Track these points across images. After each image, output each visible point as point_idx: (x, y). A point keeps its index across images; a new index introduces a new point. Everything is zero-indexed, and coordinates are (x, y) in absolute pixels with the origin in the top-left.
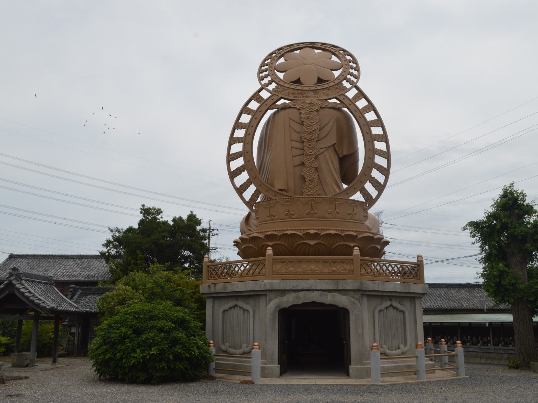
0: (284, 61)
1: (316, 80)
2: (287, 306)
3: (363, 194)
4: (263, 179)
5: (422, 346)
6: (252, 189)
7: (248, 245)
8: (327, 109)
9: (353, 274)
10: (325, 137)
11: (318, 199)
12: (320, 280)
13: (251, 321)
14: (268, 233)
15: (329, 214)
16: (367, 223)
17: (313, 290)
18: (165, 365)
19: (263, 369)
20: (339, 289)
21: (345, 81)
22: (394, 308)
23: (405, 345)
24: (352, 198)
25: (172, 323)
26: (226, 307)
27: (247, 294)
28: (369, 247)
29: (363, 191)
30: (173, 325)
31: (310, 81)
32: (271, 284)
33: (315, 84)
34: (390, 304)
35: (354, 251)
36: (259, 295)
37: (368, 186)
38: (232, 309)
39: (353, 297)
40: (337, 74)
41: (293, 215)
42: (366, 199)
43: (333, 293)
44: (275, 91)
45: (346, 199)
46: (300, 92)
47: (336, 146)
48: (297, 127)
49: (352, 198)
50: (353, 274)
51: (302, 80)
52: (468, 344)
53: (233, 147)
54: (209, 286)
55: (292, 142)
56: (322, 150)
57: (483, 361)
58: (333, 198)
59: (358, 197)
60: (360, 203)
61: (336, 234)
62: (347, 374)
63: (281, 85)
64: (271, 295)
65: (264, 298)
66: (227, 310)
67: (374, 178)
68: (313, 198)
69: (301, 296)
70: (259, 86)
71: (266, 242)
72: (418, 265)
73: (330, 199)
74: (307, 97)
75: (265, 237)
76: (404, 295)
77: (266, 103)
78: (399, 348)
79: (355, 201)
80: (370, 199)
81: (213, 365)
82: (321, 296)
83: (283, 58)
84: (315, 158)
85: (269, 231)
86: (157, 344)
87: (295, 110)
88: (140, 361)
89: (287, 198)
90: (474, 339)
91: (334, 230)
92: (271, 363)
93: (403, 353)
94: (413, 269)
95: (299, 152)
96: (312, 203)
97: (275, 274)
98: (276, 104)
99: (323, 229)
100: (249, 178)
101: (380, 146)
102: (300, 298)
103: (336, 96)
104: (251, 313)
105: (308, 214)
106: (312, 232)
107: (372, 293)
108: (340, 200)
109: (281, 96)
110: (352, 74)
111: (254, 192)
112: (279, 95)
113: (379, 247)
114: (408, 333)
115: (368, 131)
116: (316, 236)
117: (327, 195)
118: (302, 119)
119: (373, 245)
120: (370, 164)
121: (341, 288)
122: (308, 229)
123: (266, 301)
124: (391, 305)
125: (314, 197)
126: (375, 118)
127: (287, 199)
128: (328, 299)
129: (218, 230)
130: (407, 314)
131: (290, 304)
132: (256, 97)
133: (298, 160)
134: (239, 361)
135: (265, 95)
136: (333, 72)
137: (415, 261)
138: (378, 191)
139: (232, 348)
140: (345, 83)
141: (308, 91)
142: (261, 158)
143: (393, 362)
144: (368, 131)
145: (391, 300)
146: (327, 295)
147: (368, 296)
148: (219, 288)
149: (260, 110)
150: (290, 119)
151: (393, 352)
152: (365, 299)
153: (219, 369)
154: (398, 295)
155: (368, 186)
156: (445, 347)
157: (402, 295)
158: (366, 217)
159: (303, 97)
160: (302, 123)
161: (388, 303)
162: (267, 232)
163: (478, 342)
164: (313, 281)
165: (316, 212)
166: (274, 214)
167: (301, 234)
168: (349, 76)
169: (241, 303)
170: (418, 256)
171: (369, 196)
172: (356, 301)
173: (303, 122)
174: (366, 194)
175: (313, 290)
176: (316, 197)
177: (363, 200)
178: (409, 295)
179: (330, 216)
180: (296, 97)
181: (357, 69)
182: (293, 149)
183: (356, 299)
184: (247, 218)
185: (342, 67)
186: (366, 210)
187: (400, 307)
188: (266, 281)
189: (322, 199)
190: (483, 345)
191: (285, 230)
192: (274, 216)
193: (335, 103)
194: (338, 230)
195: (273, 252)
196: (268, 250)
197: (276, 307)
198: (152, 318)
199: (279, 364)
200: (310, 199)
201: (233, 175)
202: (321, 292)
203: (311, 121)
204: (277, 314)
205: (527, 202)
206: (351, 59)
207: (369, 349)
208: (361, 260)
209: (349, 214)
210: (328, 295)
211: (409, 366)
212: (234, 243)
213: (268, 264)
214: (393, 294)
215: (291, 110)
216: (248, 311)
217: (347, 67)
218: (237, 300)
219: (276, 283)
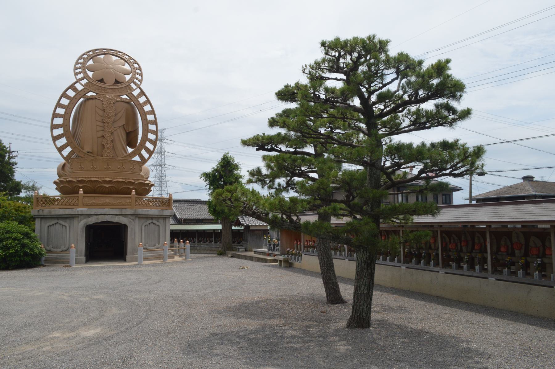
0: (93, 63)
1: (114, 81)
2: (91, 223)
4: (76, 143)
6: (68, 150)
7: (65, 185)
8: (120, 102)
9: (131, 205)
10: (118, 120)
13: (68, 232)
14: (79, 179)
16: (142, 173)
18: (18, 259)
19: (76, 259)
21: (133, 83)
22: (154, 224)
23: (159, 244)
24: (133, 159)
25: (22, 235)
26: (50, 224)
27: (66, 216)
30: (22, 236)
31: (110, 82)
32: (82, 211)
33: (113, 84)
36: (74, 217)
37: (144, 152)
38: (55, 225)
39: (130, 218)
40: (128, 77)
44: (86, 86)
46: (103, 89)
47: (125, 126)
48: (101, 112)
49: (133, 159)
50: (131, 205)
51: (105, 80)
52: (201, 242)
53: (55, 119)
54: (38, 211)
55: (97, 122)
56: (115, 129)
57: (208, 252)
59: (137, 158)
61: (122, 181)
62: (125, 260)
63: (90, 82)
64: (82, 217)
65: (76, 219)
66: (51, 226)
67: (147, 147)
70: (75, 80)
71: (78, 184)
72: (169, 200)
74: (107, 93)
75: (77, 181)
76: (160, 216)
77: (79, 93)
78: (155, 246)
79: (135, 161)
81: (43, 259)
83: (91, 60)
84: (111, 134)
85: (80, 178)
86: (14, 247)
87: (99, 101)
88: (3, 257)
90: (205, 239)
91: (121, 178)
92: (80, 256)
95: (102, 129)
97: (84, 205)
98: (87, 95)
100: (66, 142)
101: (152, 127)
103: (127, 94)
104: (68, 228)
106: (108, 179)
107: (141, 216)
109: (91, 90)
110: (137, 79)
112: (89, 89)
113: (147, 188)
114: (161, 237)
115: (145, 118)
116: (110, 182)
117: (118, 157)
118: (104, 108)
119: (143, 187)
120: (145, 138)
122: (105, 178)
123: (78, 221)
124: (152, 222)
126: (150, 109)
128: (116, 220)
129: (17, 152)
130: (161, 227)
131: (93, 223)
132: (72, 87)
133: (100, 134)
134: (59, 256)
135: (79, 87)
136: (125, 76)
139: (54, 248)
140: (133, 85)
141: (108, 89)
142: (75, 128)
143: (151, 253)
144: (145, 118)
145: (152, 219)
148: (46, 212)
149: (75, 98)
150: (96, 106)
151: (151, 248)
152: (137, 220)
153: (47, 261)
154: (157, 216)
155: (144, 152)
156: (182, 244)
157: (158, 216)
159: (105, 93)
160: (104, 110)
161: (150, 221)
162: (78, 178)
163: (207, 241)
164: (107, 209)
166: (83, 167)
168: (135, 80)
169: (61, 222)
172: (132, 221)
173: (104, 110)
175: (107, 215)
177: (140, 160)
178: (162, 216)
179: (119, 170)
180: (100, 92)
181: (141, 75)
182: (97, 126)
183: (132, 219)
184: (64, 166)
185: (132, 73)
186: (141, 166)
187: (157, 223)
188: (78, 209)
190: (210, 243)
191: (90, 178)
192: (83, 168)
193: (126, 98)
195: (83, 192)
197: (84, 224)
198: (7, 232)
201: (55, 139)
203: (110, 110)
204: (85, 228)
205: (235, 163)
206: (138, 67)
207: (138, 246)
208: (136, 197)
209: (130, 169)
211: (160, 255)
214: (154, 216)
215: (97, 100)
216: (65, 226)
217: (135, 73)
218: (58, 219)
219: (85, 210)
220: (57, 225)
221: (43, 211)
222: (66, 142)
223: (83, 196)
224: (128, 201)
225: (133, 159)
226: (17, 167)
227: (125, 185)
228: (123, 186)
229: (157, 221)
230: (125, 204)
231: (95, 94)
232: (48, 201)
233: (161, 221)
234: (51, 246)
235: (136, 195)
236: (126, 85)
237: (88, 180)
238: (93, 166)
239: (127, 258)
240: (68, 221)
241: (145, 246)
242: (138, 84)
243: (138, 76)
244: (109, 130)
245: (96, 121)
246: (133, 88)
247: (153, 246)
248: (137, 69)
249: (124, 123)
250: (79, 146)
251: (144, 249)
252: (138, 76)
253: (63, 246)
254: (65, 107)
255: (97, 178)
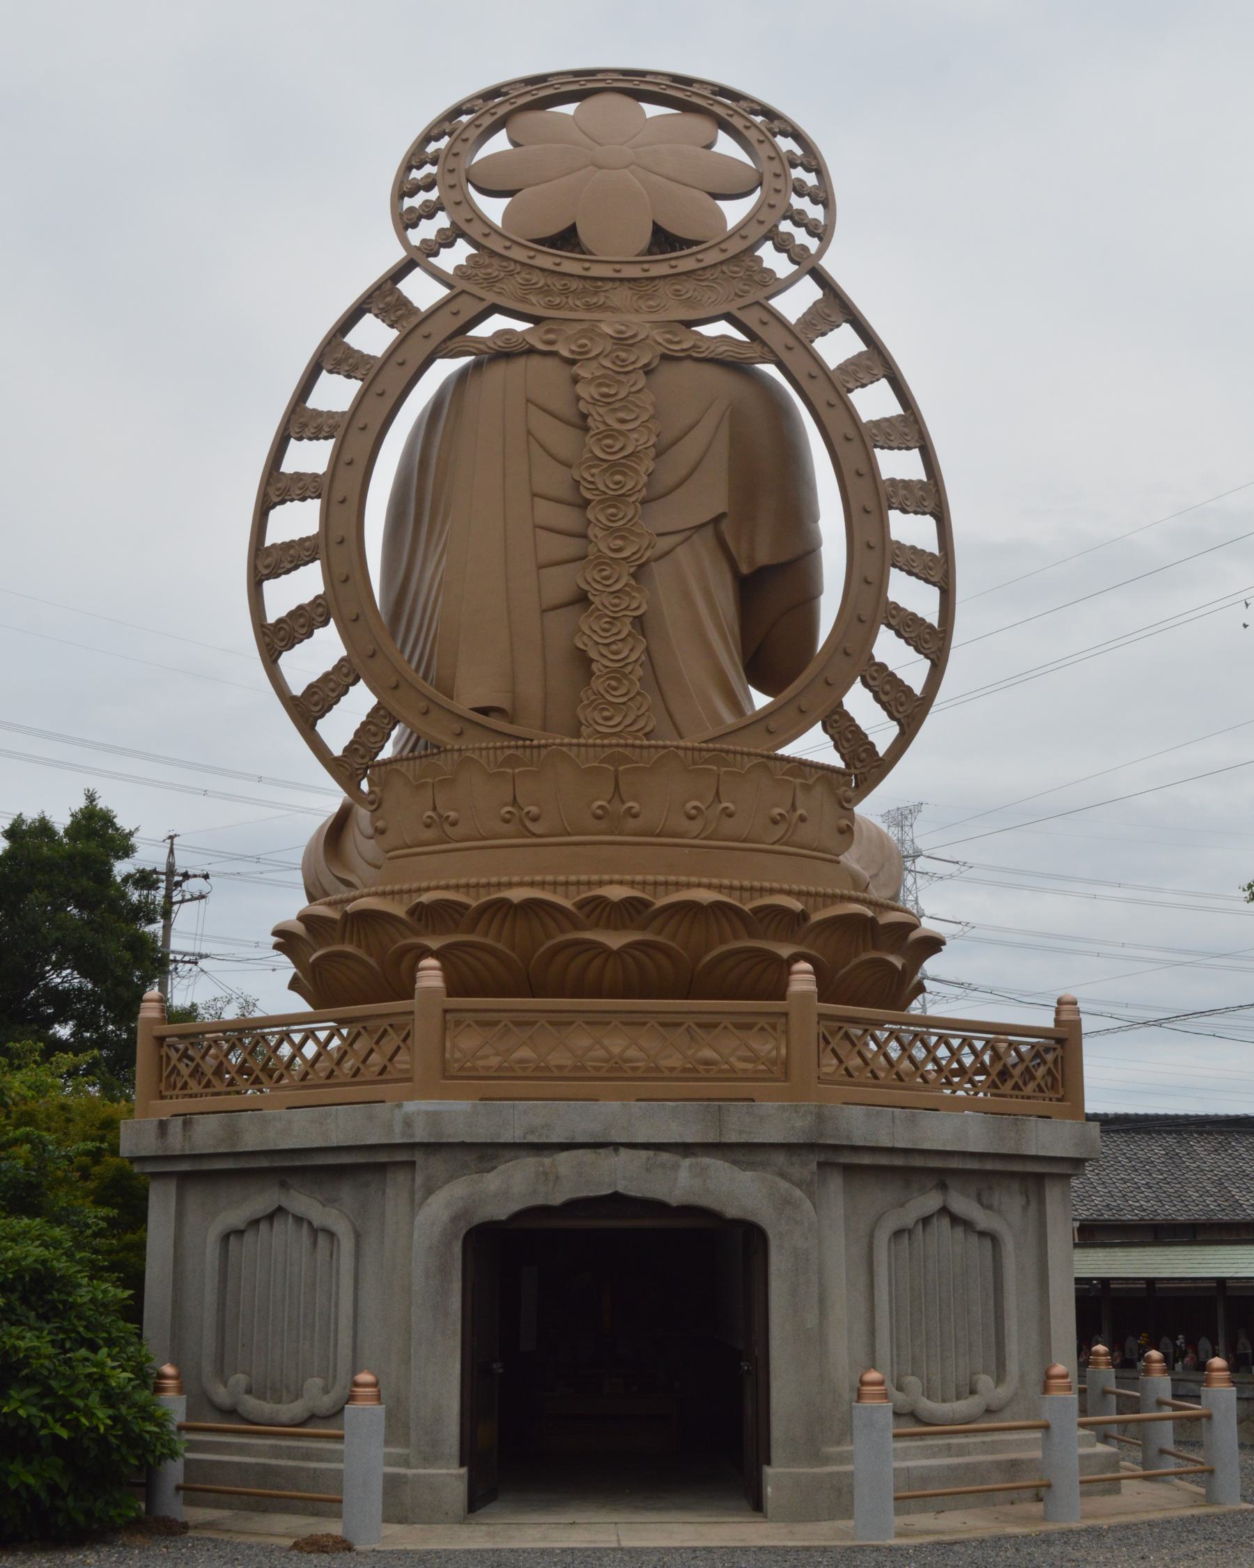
1: (644, 237)
2: (501, 1212)
3: (836, 736)
5: (1069, 1380)
8: (688, 366)
9: (786, 1076)
11: (645, 752)
12: (903, 1108)
14: (425, 898)
15: (691, 818)
16: (851, 859)
17: (616, 1146)
19: (392, 1485)
20: (725, 1140)
21: (769, 244)
22: (955, 1220)
23: (1000, 1378)
26: (236, 1216)
28: (855, 961)
29: (836, 721)
34: (942, 1205)
35: (794, 977)
36: (382, 1168)
38: (263, 1227)
39: (782, 1175)
40: (735, 212)
41: (535, 819)
42: (847, 757)
43: (700, 1160)
45: (763, 756)
46: (574, 285)
47: (725, 526)
48: (561, 439)
51: (584, 234)
53: (276, 515)
54: (163, 1126)
56: (664, 544)
58: (708, 750)
60: (821, 773)
62: (757, 1504)
63: (493, 254)
65: (401, 1177)
66: (240, 1233)
67: (882, 667)
68: (620, 750)
69: (563, 1170)
70: (399, 254)
71: (416, 933)
72: (1060, 1041)
73: (696, 753)
74: (602, 308)
75: (411, 912)
76: (999, 1166)
77: (424, 330)
78: (973, 1392)
79: (801, 766)
80: (864, 755)
81: (174, 1472)
82: (648, 1170)
84: (634, 576)
85: (428, 889)
87: (551, 363)
89: (509, 747)
91: (709, 886)
92: (427, 1460)
93: (989, 1412)
94: (1037, 1055)
95: (569, 547)
96: (616, 771)
99: (661, 884)
100: (344, 653)
102: (557, 1178)
103: (732, 308)
104: (346, 1244)
105: (599, 818)
106: (616, 893)
107: (866, 1160)
108: (739, 757)
110: (799, 219)
111: (368, 716)
113: (897, 962)
115: (864, 469)
116: (631, 911)
117: (682, 737)
118: (583, 407)
121: (733, 1138)
122: (601, 884)
124: (944, 1211)
125: (626, 746)
127: (512, 751)
129: (206, 877)
130: (1009, 1246)
131: (515, 1207)
133: (560, 584)
134: (291, 1453)
137: (1046, 1020)
138: (900, 723)
139: (261, 1396)
140: (773, 259)
141: (609, 285)
144: (864, 469)
145: (943, 1187)
146: (676, 1167)
147: (848, 1169)
149: (398, 358)
150: (528, 401)
151: (946, 1407)
152: (835, 1183)
156: (1161, 1383)
157: (989, 1166)
158: (847, 832)
159: (589, 307)
160: (582, 423)
161: (931, 1202)
162: (419, 890)
164: (616, 1105)
165: (634, 811)
166: (453, 815)
167: (567, 904)
168: (786, 226)
169: (302, 1202)
170: (1060, 1002)
171: (861, 746)
172: (798, 1193)
173: (584, 417)
174: (850, 736)
175: (616, 1146)
176: (633, 746)
177: (835, 760)
179: (696, 826)
180: (558, 307)
181: (823, 197)
183: (798, 1185)
185: (760, 184)
186: (845, 805)
187: (982, 1219)
188: (411, 1107)
189: (662, 752)
191: (499, 885)
193: (724, 338)
194: (726, 887)
195: (447, 979)
196: (424, 969)
197: (455, 1219)
199: (462, 1465)
200: (608, 751)
202: (651, 1153)
203: (622, 415)
204: (457, 1248)
206: (799, 151)
208: (822, 1017)
210: (679, 1166)
211: (1014, 1464)
212: (275, 939)
213: (425, 1028)
214: (955, 1164)
215: (535, 361)
216: (331, 1235)
217: (779, 184)
218: (283, 1185)
220: (278, 1224)
221: (187, 1124)
222: (344, 653)
223: (446, 1011)
224: (765, 1047)
225: (786, 751)
226: (207, 956)
227: (736, 937)
228: (723, 941)
229: (980, 1201)
230: (745, 1071)
231: (521, 326)
232: (257, 1072)
233: (1011, 1203)
234: (239, 1380)
235: (823, 996)
236: (723, 257)
237: (485, 898)
238: (514, 802)
239: (769, 1490)
240: (347, 1192)
241: (899, 1396)
242: (804, 248)
243: (799, 203)
244: (620, 550)
245: (535, 495)
246: (770, 272)
247: (958, 1398)
248: (794, 166)
249: (720, 506)
250: (425, 678)
251: (897, 1414)
252: (799, 203)
253: (318, 1381)
254: (336, 427)
255: (542, 884)
